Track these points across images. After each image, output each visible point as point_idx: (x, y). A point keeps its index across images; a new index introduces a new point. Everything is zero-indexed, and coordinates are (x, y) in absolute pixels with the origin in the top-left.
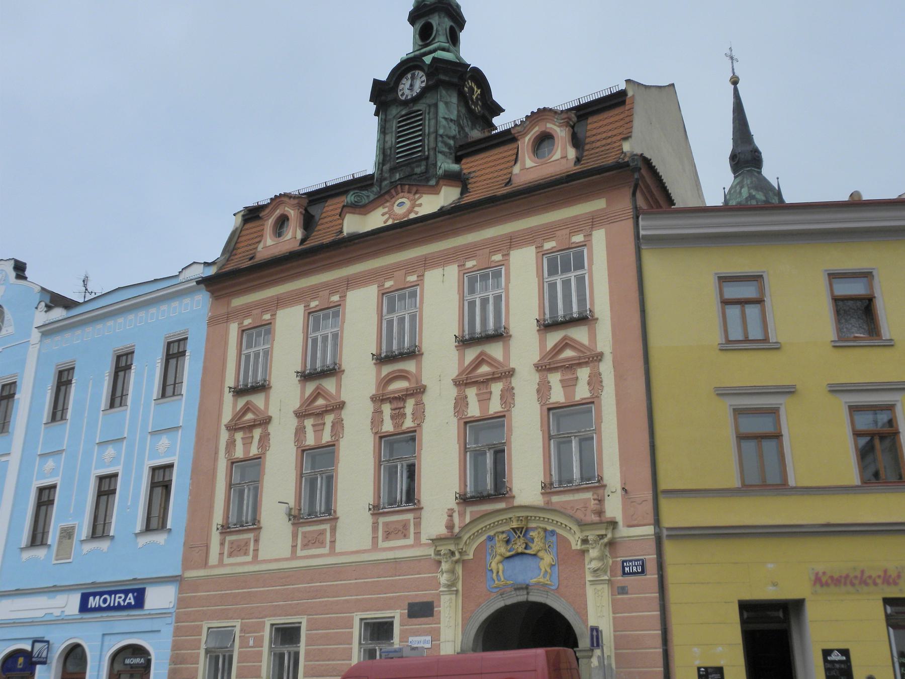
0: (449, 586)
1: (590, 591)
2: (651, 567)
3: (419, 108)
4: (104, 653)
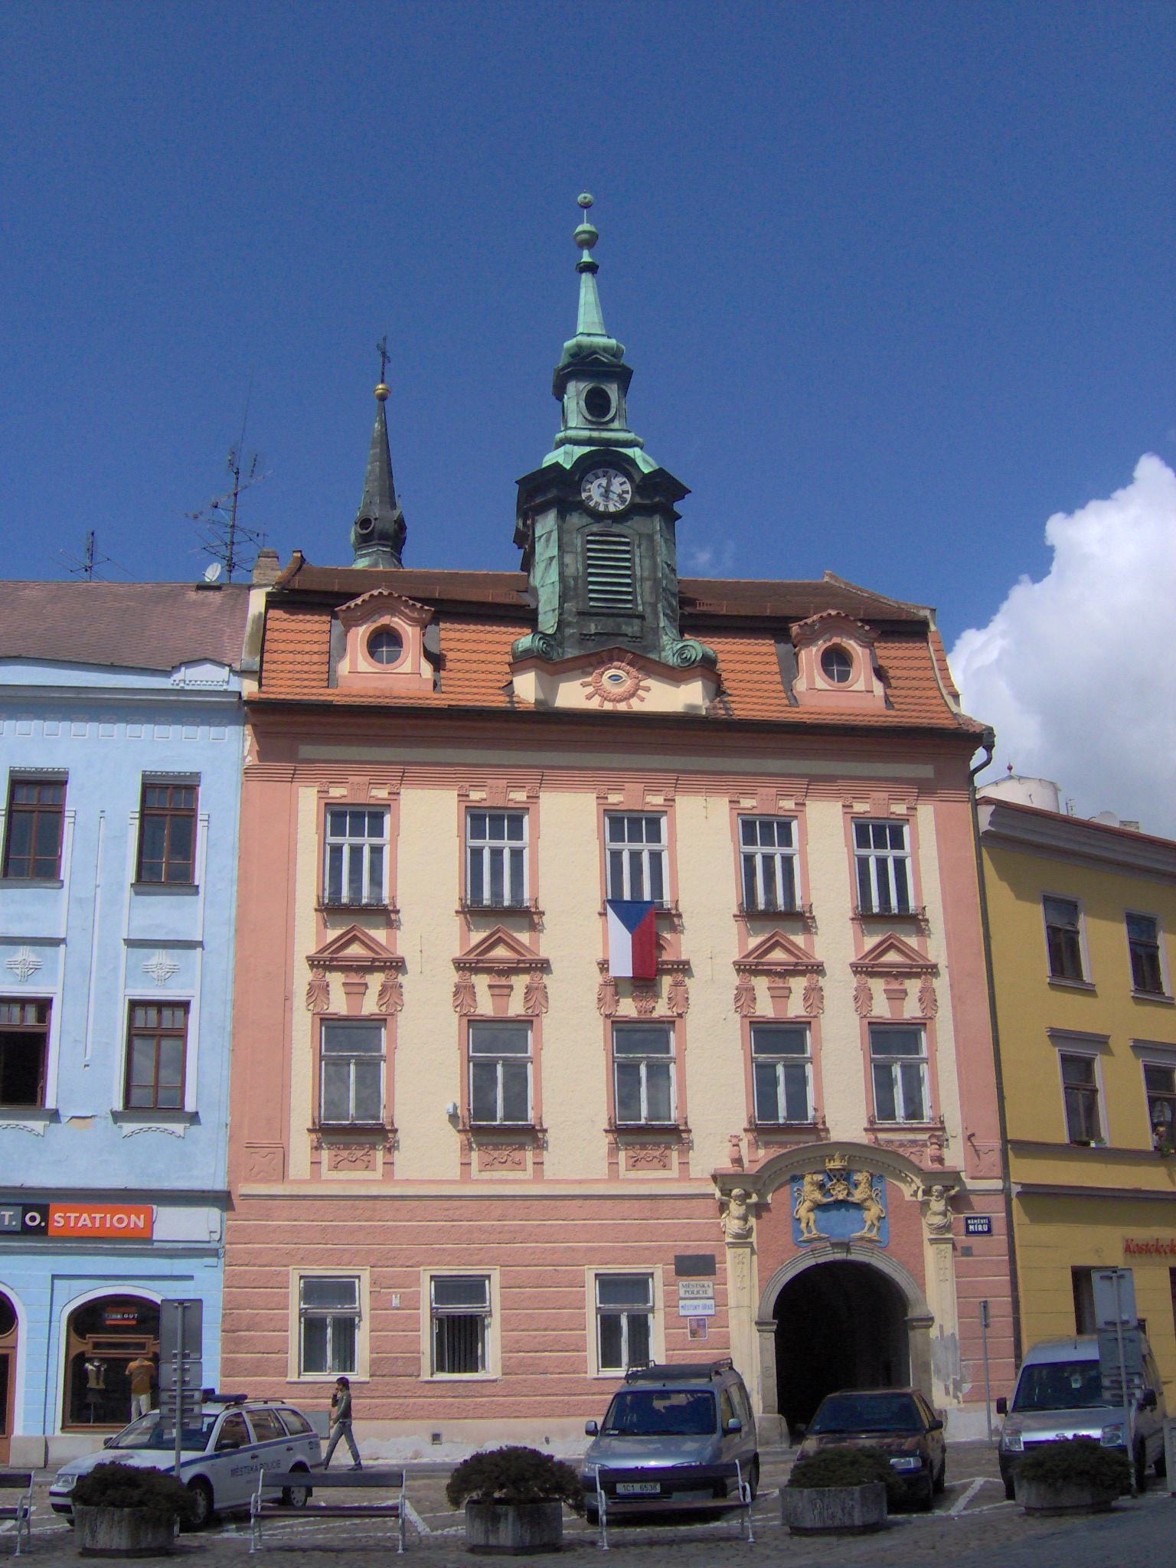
0: (737, 1236)
1: (930, 1252)
2: (999, 1226)
3: (625, 531)
4: (56, 1309)
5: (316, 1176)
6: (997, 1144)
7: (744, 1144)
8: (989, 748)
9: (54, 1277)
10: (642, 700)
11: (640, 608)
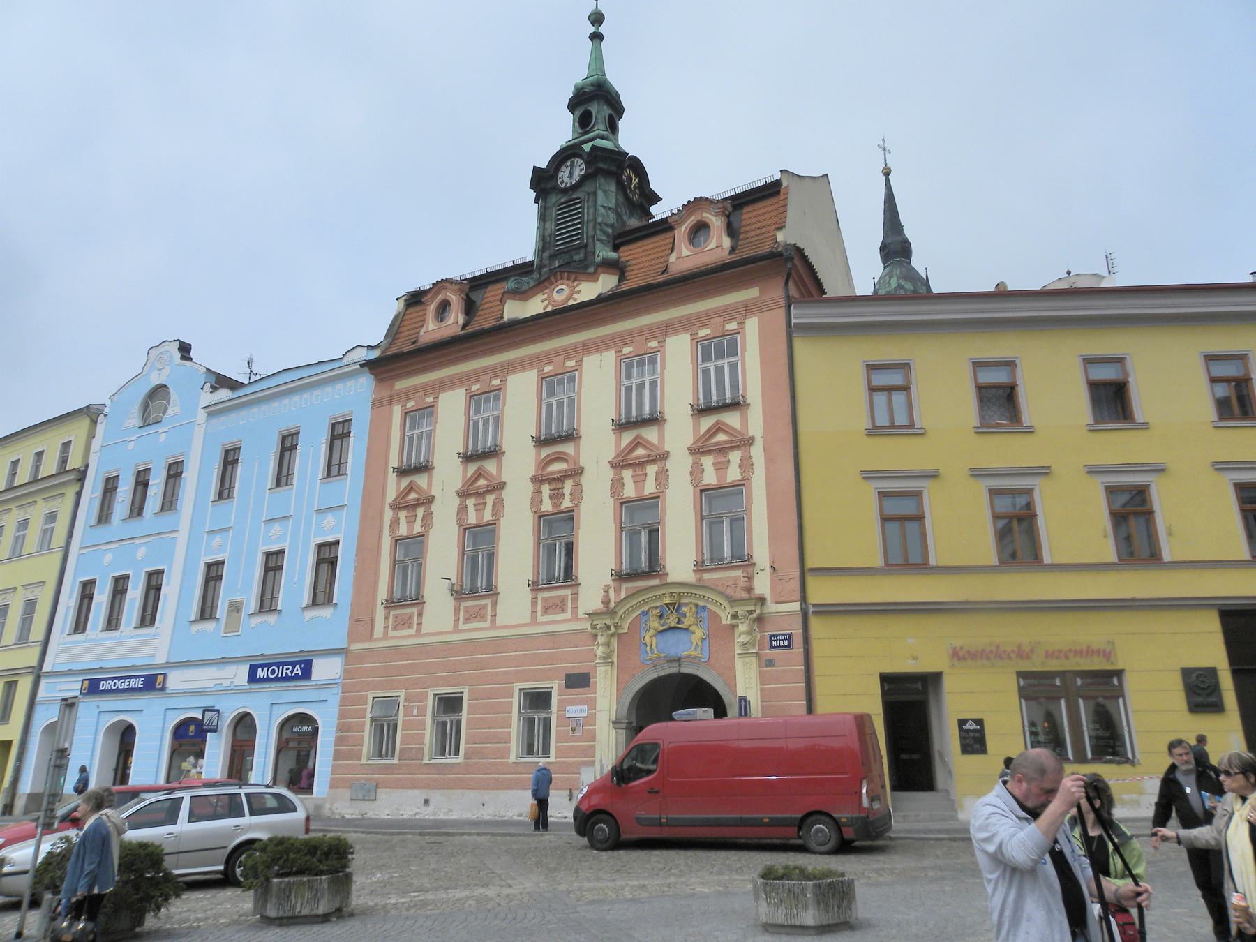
0: (604, 658)
1: (739, 663)
4: (274, 717)
6: (796, 573)
7: (612, 592)
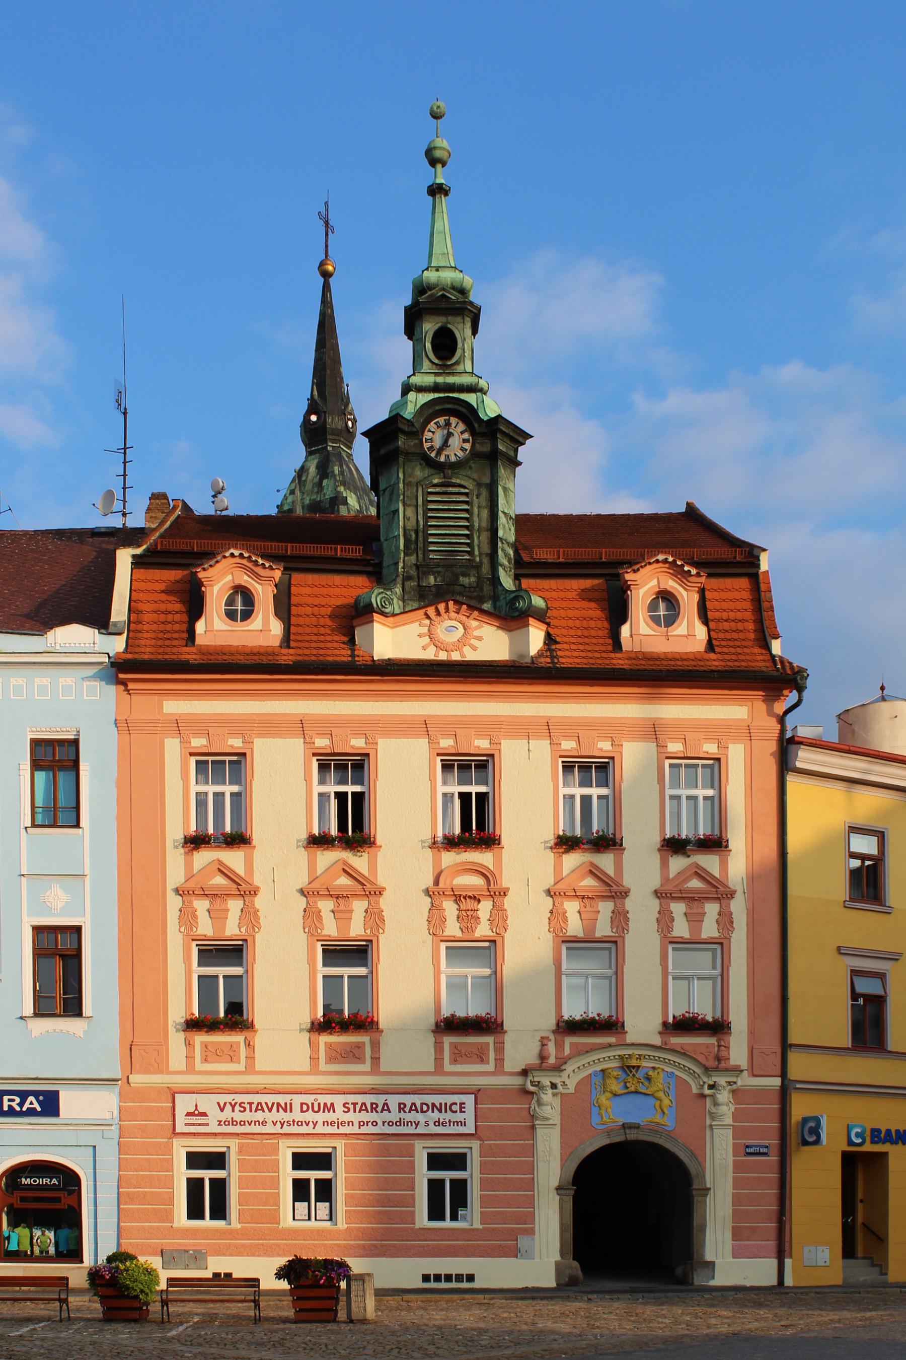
5: (190, 1069)
8: (800, 689)
9: (95, 1147)
10: (474, 648)
11: (478, 559)
